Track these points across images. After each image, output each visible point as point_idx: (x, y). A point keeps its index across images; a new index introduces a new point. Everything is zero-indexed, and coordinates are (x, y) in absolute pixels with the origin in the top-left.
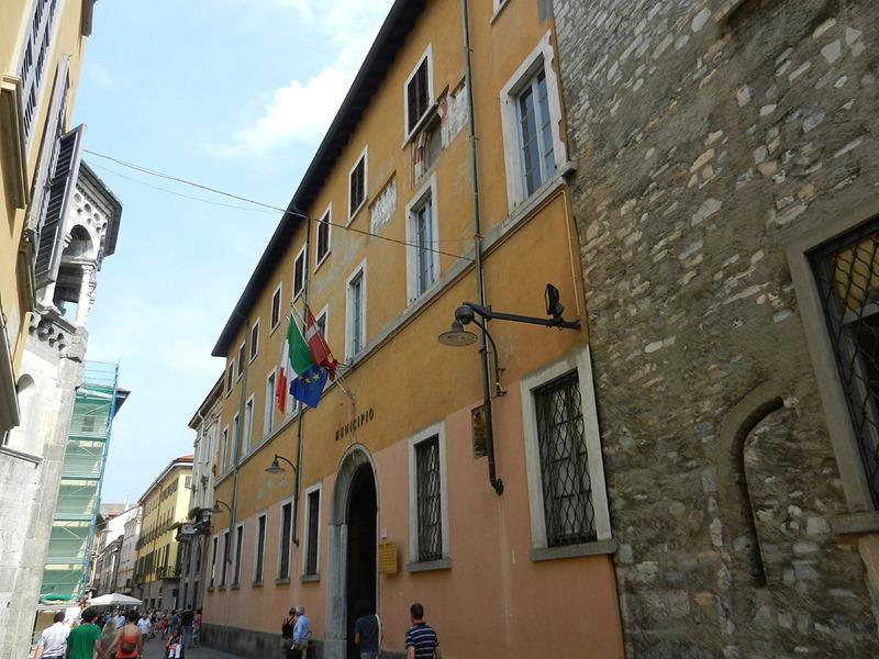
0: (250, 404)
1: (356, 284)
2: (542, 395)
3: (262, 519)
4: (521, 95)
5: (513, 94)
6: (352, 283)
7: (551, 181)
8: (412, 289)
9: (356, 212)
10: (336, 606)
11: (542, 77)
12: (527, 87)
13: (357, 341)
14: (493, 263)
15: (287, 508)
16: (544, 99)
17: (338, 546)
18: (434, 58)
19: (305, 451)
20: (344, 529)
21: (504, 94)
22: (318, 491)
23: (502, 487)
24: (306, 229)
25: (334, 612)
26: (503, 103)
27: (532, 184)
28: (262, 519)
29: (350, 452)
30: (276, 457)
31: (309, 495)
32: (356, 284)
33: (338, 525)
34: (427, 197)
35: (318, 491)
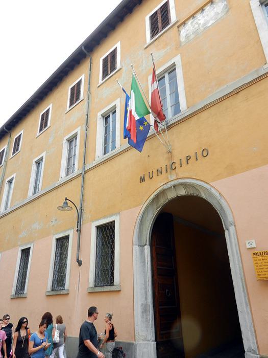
0: (10, 182)
1: (70, 141)
2: (100, 228)
3: (26, 252)
4: (106, 117)
5: (103, 116)
6: (103, 116)
7: (77, 170)
8: (63, 172)
9: (42, 132)
10: (145, 311)
11: (76, 139)
12: (173, 68)
13: (7, 204)
14: (87, 175)
15: (62, 242)
16: (114, 121)
17: (144, 262)
18: (85, 80)
19: (87, 197)
20: (147, 249)
21: (99, 114)
22: (30, 248)
23: (81, 264)
24: (89, 60)
25: (142, 317)
26: (98, 118)
27: (68, 170)
28: (26, 252)
29: (166, 187)
30: (66, 199)
31: (98, 227)
32: (38, 163)
33: (142, 246)
34: (41, 159)
35: (30, 248)
